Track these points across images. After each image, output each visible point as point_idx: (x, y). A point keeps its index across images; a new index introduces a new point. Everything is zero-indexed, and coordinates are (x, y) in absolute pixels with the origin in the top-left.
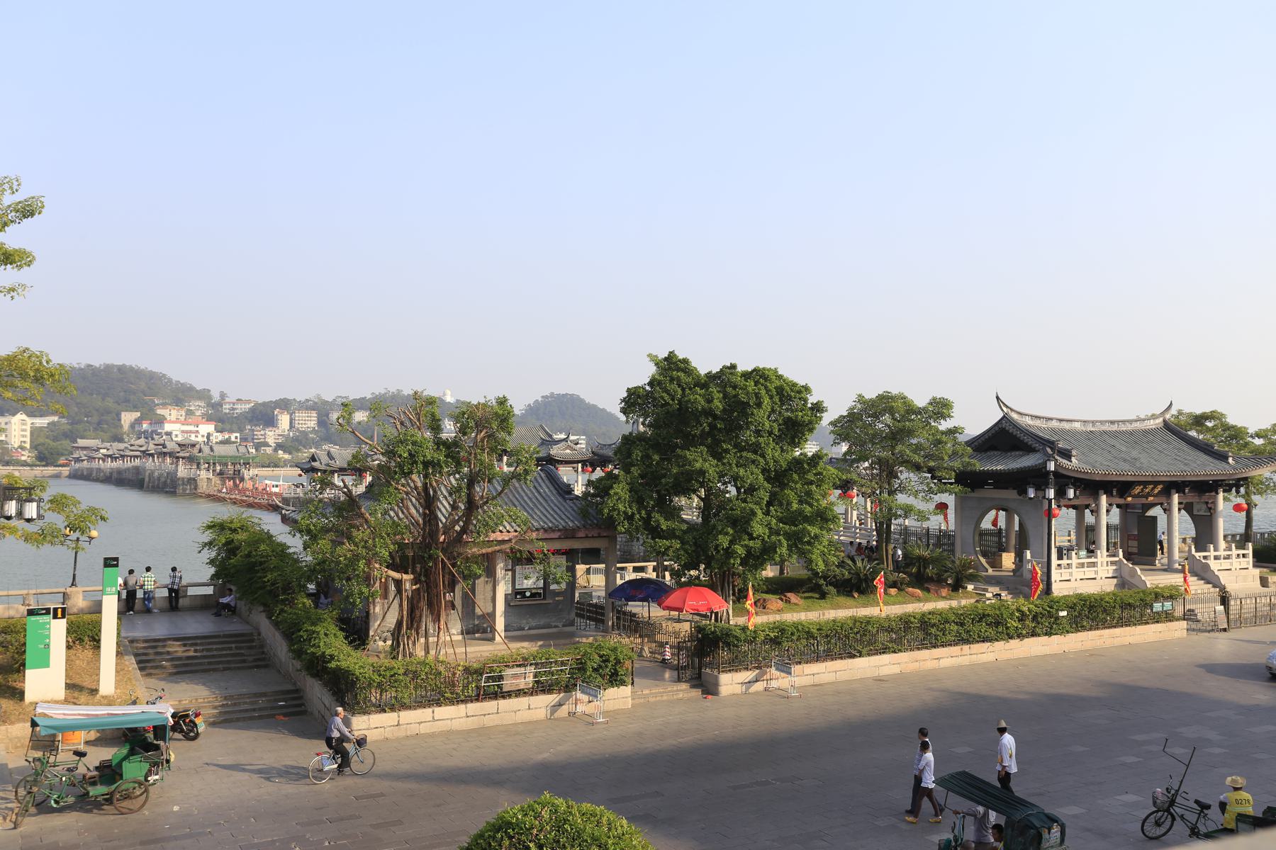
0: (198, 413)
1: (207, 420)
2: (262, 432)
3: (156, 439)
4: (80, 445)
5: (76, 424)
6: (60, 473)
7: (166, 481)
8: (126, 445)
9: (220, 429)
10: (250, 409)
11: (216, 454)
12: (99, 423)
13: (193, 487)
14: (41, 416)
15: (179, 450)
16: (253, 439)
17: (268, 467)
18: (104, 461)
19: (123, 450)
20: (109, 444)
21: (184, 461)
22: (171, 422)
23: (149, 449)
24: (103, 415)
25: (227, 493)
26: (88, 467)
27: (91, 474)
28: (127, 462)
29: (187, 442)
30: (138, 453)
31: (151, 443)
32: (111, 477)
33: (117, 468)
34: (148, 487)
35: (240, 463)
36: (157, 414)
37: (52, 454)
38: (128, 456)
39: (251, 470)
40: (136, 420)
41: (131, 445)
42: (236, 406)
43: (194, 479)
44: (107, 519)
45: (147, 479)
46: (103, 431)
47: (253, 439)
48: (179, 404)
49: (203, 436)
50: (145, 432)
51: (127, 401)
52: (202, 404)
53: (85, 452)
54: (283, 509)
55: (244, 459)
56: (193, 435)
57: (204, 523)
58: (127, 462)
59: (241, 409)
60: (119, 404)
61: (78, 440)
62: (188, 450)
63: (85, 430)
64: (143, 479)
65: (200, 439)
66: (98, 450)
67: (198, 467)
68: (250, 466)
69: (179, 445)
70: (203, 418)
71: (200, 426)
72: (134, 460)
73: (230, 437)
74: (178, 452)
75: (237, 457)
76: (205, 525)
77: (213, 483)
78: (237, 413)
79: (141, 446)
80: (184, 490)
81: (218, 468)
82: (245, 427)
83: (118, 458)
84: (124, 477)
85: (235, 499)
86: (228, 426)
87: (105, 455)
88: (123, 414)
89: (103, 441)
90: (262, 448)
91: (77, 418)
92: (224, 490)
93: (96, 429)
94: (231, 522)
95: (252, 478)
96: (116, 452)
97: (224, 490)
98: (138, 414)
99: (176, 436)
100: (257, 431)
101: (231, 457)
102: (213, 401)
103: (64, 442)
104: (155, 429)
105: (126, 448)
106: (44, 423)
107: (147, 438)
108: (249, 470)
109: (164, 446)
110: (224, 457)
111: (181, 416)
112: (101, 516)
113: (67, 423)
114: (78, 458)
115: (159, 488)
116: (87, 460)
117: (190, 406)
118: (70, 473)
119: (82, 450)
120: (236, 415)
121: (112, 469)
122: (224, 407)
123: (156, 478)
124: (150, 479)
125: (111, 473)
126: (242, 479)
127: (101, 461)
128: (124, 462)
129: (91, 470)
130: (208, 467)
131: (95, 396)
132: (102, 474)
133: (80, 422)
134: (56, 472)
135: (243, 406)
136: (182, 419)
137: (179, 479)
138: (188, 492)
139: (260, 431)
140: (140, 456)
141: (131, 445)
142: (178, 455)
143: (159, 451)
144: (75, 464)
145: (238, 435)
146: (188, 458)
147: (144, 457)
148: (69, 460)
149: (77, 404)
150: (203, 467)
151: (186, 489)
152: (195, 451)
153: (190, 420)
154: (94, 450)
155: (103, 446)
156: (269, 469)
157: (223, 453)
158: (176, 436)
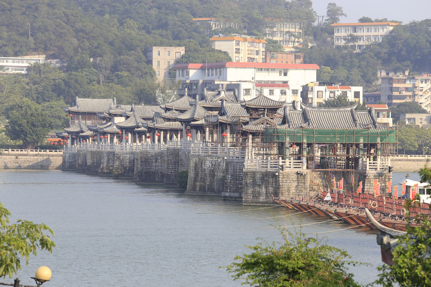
0: (288, 48)
1: (305, 62)
2: (409, 84)
3: (209, 98)
4: (81, 109)
5: (76, 69)
6: (48, 160)
7: (224, 178)
8: (157, 109)
9: (327, 78)
10: (385, 37)
11: (314, 126)
12: (115, 68)
13: (271, 189)
14: (16, 54)
15: (247, 119)
16: (390, 97)
17: (419, 152)
18: (120, 139)
19: (152, 119)
20: (129, 107)
21: (258, 140)
22: (240, 65)
23: (196, 116)
24: (120, 54)
25: (332, 203)
26: (95, 149)
27: (99, 163)
28: (159, 140)
29: (262, 103)
30: (177, 125)
31: (200, 104)
32: (131, 169)
33: (141, 153)
34: (194, 188)
35: (357, 145)
36: (213, 50)
37: (34, 125)
38: (160, 130)
39: (379, 159)
40: (177, 62)
41: (167, 110)
42: (359, 33)
43: (274, 176)
44: (52, 244)
45: (191, 174)
46: (121, 83)
47: (390, 97)
48: (255, 31)
49: (295, 92)
50: (194, 83)
51: (163, 26)
52: (295, 29)
53: (89, 122)
54: (384, 233)
55: (364, 137)
56: (277, 91)
57: (236, 258)
58: (159, 140)
59: (368, 38)
60: (149, 32)
61: (79, 100)
62: (262, 118)
63: (91, 81)
64: (185, 175)
65: (289, 98)
66: (110, 117)
67: (281, 153)
68: (376, 151)
69: (248, 109)
70: (296, 57)
71: (291, 73)
72: (171, 138)
73: (345, 94)
74: (246, 123)
75: (353, 133)
76: (240, 261)
77: (308, 183)
78: (360, 46)
79: (182, 111)
80: (256, 195)
81: (318, 154)
82: (375, 74)
83: (144, 133)
84: (153, 169)
85: (347, 214)
86: (342, 73)
87: (122, 128)
88: (155, 50)
89: (120, 102)
90: (408, 116)
91: (76, 58)
92: (328, 198)
93: (108, 79)
94: (288, 257)
95: (380, 175)
96: (141, 121)
97: (328, 198)
98: (182, 50)
99: (247, 91)
100: (399, 81)
101: (342, 133)
102: (316, 24)
103: (54, 103)
104: (210, 78)
105: (158, 114)
106: (21, 68)
107: (194, 97)
108: (375, 159)
109: (221, 111)
110: (327, 133)
111: (257, 53)
112: (42, 240)
113: (60, 68)
114: (78, 133)
115: (212, 190)
116: (93, 136)
117: (273, 34)
118: (64, 162)
119: (83, 119)
120: (358, 51)
121: (132, 153)
122: (336, 34)
123: (207, 172)
124: (197, 174)
125: (132, 162)
126: (363, 177)
127: (115, 140)
128: (153, 140)
129: (97, 155)
130: (300, 152)
131: (107, 16)
132: (117, 163)
133: (82, 65)
134: (40, 159)
135: (373, 33)
136: (259, 58)
137: (246, 174)
138: (262, 199)
139: (404, 81)
140: (181, 130)
141: (167, 110)
142: (245, 128)
143: (213, 120)
144: (72, 143)
145: (360, 89)
146: (263, 134)
147: (188, 131)
148: (63, 138)
149: (77, 31)
150: (288, 152)
151: (259, 194)
152: (277, 121)
153: (274, 61)
154: (104, 118)
155: (118, 111)
156: (421, 158)
157: (326, 126)
158: (247, 91)
